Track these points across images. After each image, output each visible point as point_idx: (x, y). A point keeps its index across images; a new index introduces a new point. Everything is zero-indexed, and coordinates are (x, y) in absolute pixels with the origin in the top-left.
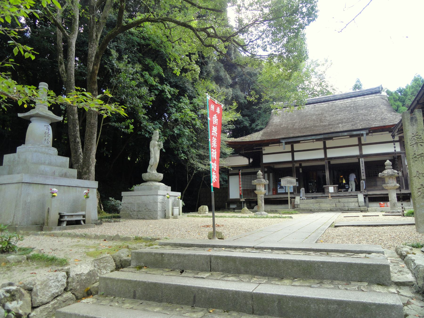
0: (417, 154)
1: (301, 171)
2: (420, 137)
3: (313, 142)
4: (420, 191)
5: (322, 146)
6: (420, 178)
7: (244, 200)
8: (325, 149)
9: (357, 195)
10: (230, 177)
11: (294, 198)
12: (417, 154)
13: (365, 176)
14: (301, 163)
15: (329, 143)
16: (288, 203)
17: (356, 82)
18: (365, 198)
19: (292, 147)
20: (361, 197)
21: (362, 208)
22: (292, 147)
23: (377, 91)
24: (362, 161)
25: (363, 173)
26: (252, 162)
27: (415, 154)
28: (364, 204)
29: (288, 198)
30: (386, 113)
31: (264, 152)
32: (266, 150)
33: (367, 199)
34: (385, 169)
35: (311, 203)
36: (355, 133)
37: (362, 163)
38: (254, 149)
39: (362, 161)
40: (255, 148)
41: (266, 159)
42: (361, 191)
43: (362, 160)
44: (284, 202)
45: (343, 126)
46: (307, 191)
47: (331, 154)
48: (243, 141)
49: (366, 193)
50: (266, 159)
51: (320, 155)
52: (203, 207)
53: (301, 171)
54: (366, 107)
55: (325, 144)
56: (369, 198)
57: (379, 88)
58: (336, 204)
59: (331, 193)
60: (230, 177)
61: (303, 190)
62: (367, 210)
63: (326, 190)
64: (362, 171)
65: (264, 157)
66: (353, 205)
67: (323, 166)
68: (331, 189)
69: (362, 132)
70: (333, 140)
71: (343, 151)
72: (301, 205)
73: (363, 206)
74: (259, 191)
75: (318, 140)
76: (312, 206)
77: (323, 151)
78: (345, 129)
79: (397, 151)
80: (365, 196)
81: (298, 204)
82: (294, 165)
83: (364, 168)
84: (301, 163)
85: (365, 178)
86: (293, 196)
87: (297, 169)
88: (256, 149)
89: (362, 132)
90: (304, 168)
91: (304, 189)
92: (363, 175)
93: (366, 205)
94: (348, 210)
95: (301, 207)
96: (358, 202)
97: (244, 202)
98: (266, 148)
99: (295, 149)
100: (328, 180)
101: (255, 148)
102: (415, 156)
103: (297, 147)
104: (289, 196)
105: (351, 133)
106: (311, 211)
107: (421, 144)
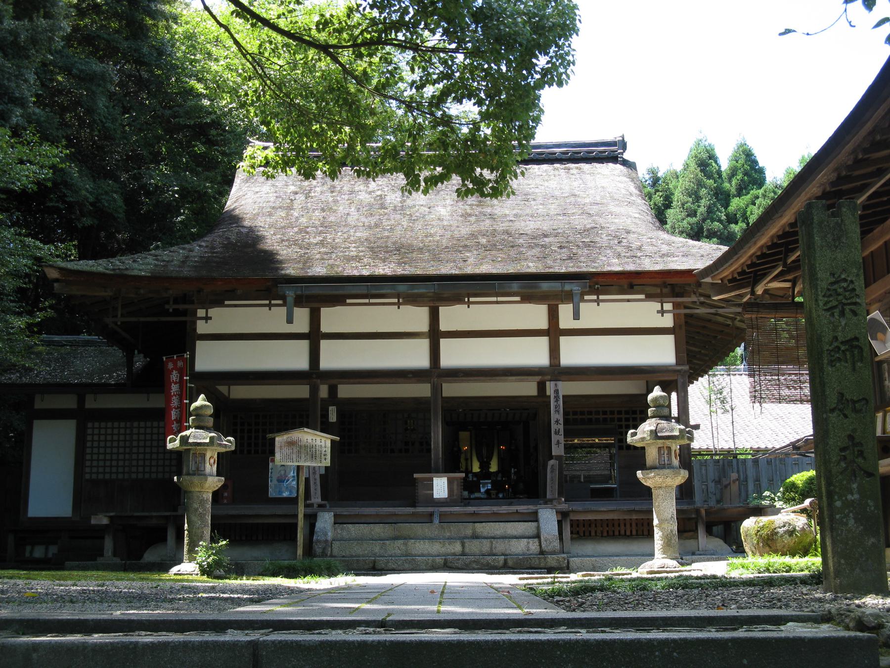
0: (840, 339)
2: (851, 287)
4: (845, 458)
5: (423, 326)
6: (846, 416)
7: (105, 521)
8: (435, 335)
10: (36, 423)
12: (840, 339)
14: (334, 381)
18: (559, 522)
20: (548, 519)
21: (551, 560)
23: (609, 153)
27: (836, 338)
28: (556, 544)
29: (296, 516)
31: (202, 328)
36: (545, 286)
40: (171, 308)
41: (210, 358)
44: (284, 533)
47: (454, 354)
49: (564, 507)
50: (210, 358)
51: (415, 355)
56: (575, 525)
57: (614, 144)
59: (441, 503)
60: (36, 423)
62: (568, 568)
63: (422, 492)
64: (554, 427)
65: (200, 345)
68: (440, 487)
69: (568, 286)
70: (469, 303)
72: (336, 545)
74: (196, 479)
80: (563, 516)
84: (334, 381)
92: (558, 443)
96: (538, 536)
99: (325, 328)
101: (171, 308)
102: (836, 344)
107: (853, 307)
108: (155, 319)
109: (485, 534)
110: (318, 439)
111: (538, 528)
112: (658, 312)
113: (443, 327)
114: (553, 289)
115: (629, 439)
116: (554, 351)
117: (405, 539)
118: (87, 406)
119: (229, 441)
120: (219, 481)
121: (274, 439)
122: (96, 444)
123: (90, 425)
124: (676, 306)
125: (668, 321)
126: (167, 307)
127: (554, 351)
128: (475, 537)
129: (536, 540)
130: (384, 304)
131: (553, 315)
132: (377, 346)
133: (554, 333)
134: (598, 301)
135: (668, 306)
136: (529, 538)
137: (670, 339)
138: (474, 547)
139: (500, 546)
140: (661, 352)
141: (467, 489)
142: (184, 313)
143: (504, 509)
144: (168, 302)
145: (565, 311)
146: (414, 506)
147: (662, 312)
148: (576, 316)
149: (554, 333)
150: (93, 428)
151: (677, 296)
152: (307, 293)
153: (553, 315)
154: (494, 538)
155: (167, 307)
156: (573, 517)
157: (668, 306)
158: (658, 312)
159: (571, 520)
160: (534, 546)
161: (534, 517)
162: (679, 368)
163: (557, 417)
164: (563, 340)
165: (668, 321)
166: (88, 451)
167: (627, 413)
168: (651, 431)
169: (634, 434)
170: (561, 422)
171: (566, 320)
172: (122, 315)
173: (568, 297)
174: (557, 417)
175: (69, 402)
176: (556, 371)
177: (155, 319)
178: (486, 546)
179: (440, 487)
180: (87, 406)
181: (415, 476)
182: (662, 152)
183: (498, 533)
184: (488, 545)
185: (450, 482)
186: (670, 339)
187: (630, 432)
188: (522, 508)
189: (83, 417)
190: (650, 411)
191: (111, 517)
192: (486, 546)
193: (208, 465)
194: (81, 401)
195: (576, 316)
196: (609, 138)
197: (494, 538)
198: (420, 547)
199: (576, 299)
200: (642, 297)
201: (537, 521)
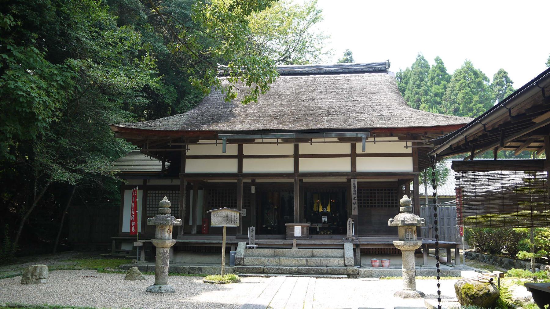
1: (253, 191)
3: (277, 143)
5: (291, 152)
7: (141, 244)
8: (297, 156)
9: (343, 245)
11: (236, 245)
13: (357, 210)
15: (304, 148)
16: (221, 253)
17: (345, 55)
19: (240, 149)
20: (349, 249)
21: (350, 270)
22: (240, 149)
23: (381, 69)
24: (354, 184)
25: (354, 204)
26: (169, 167)
30: (395, 105)
32: (193, 149)
33: (358, 251)
34: (399, 212)
35: (264, 256)
36: (348, 135)
37: (354, 187)
38: (168, 147)
39: (354, 184)
41: (192, 167)
42: (348, 236)
43: (354, 182)
45: (329, 121)
46: (260, 232)
47: (306, 166)
48: (148, 128)
49: (357, 242)
50: (192, 167)
51: (287, 166)
52: (35, 268)
53: (253, 191)
54: (363, 91)
55: (296, 148)
57: (385, 64)
58: (307, 260)
59: (298, 238)
61: (252, 229)
63: (289, 232)
64: (353, 201)
65: (188, 161)
66: (335, 263)
67: (292, 184)
68: (298, 231)
69: (360, 135)
70: (311, 143)
71: (326, 162)
72: (246, 259)
73: (351, 266)
74: (160, 241)
75: (286, 141)
76: (266, 262)
77: (291, 161)
78: (333, 126)
79: (438, 194)
81: (241, 258)
82: (240, 181)
83: (356, 196)
84: (254, 178)
85: (357, 214)
86: (233, 240)
87: (247, 187)
88: (173, 147)
89: (360, 135)
90: (259, 186)
91: (254, 228)
93: (357, 263)
94: (327, 273)
95: (246, 263)
97: (140, 247)
98: (190, 146)
100: (297, 208)
103: (248, 149)
104: (224, 240)
105: (341, 134)
106: (263, 272)
108: (164, 150)
109: (318, 255)
110: (233, 213)
111: (344, 253)
112: (405, 147)
113: (300, 153)
114: (352, 136)
115: (389, 224)
116: (354, 164)
117: (280, 256)
118: (148, 184)
119: (179, 221)
120: (173, 242)
121: (211, 213)
122: (151, 200)
123: (149, 192)
124: (413, 144)
125: (409, 150)
126: (169, 144)
127: (354, 164)
128: (313, 256)
129: (343, 259)
130: (270, 143)
131: (353, 147)
132: (270, 162)
133: (353, 156)
134: (375, 142)
135: (410, 144)
136: (340, 257)
137: (410, 159)
138: (313, 261)
139: (324, 262)
140: (405, 165)
141: (311, 232)
142: (180, 147)
143: (328, 242)
144: (169, 142)
145: (359, 146)
146: (285, 239)
147: (407, 147)
148: (364, 149)
149: (353, 156)
150: (150, 193)
151: (415, 139)
152: (232, 138)
153: (353, 147)
154: (322, 257)
155: (169, 144)
156: (361, 247)
157: (410, 144)
158: (405, 147)
159: (361, 249)
160: (341, 262)
161: (342, 247)
162: (414, 173)
163: (354, 195)
164: (358, 159)
165: (409, 150)
166: (148, 203)
167: (388, 190)
168: (402, 221)
169: (392, 221)
170: (357, 198)
171: (359, 151)
172: (149, 148)
173: (360, 140)
174: (354, 195)
175: (140, 182)
176: (354, 173)
177: (164, 150)
178: (317, 261)
179: (298, 231)
180: (148, 184)
181: (286, 224)
182: (401, 63)
183: (324, 255)
184: (319, 261)
185: (303, 228)
186: (410, 159)
187: (390, 219)
188: (336, 242)
189: (145, 188)
190: (402, 208)
191: (144, 242)
192: (317, 261)
193: (167, 234)
194: (145, 181)
195: (364, 149)
196: (383, 61)
197: (322, 257)
198: (285, 261)
199: (364, 141)
200: (396, 139)
201: (343, 249)
